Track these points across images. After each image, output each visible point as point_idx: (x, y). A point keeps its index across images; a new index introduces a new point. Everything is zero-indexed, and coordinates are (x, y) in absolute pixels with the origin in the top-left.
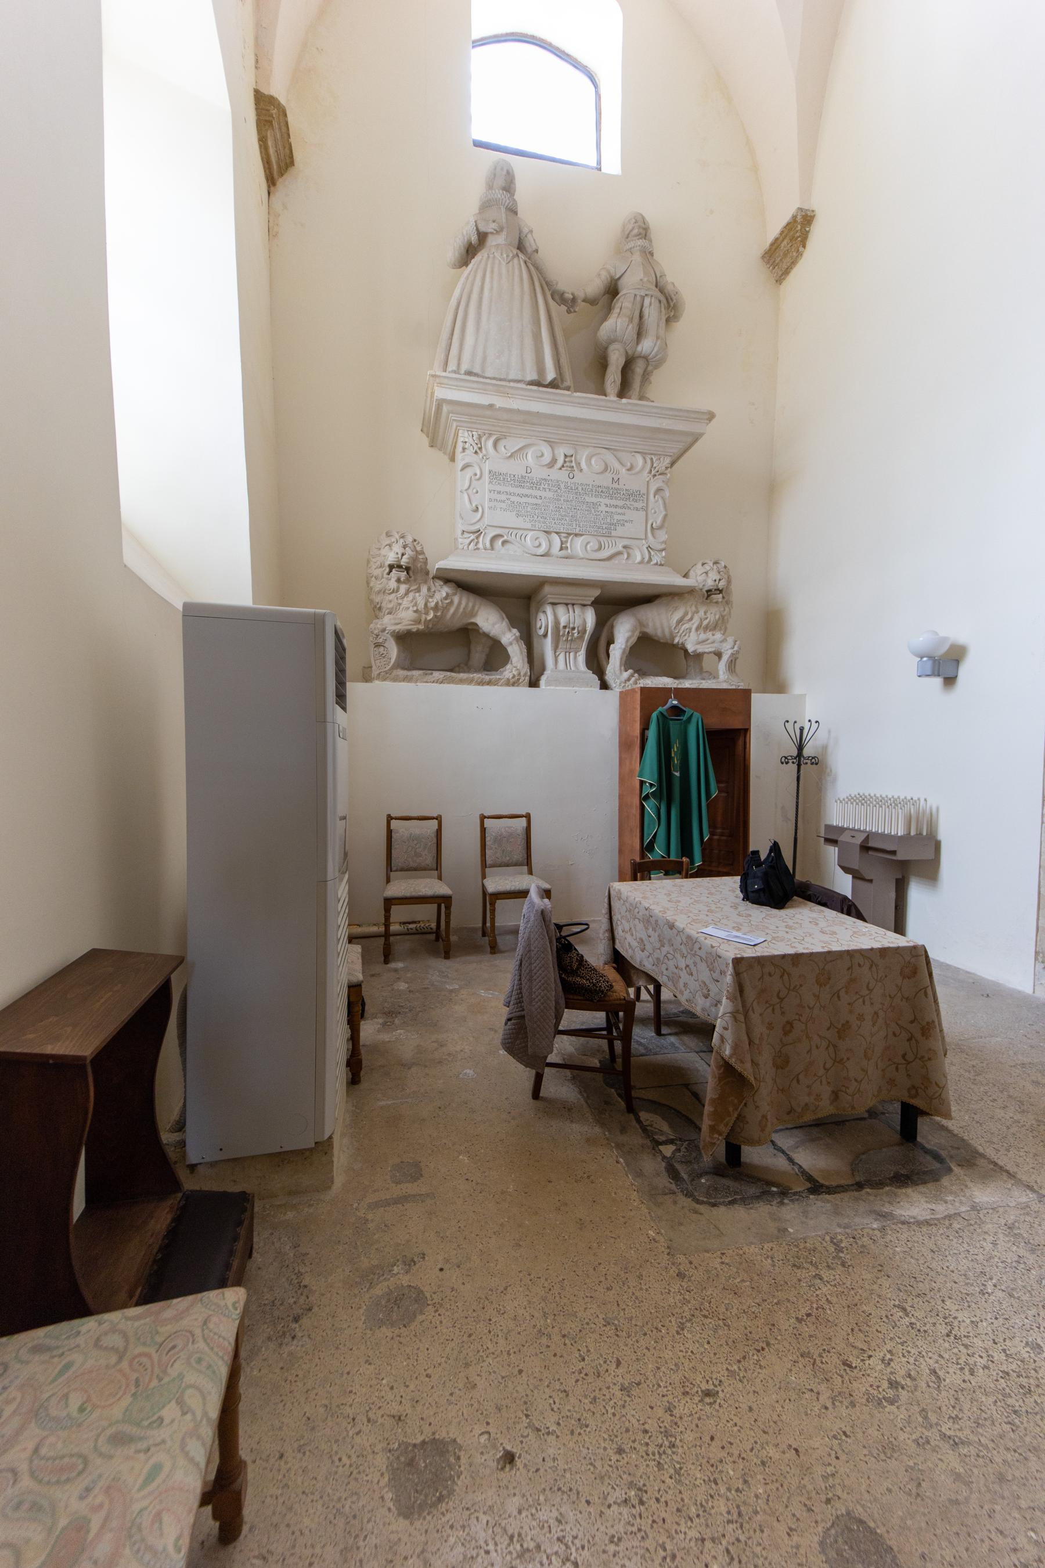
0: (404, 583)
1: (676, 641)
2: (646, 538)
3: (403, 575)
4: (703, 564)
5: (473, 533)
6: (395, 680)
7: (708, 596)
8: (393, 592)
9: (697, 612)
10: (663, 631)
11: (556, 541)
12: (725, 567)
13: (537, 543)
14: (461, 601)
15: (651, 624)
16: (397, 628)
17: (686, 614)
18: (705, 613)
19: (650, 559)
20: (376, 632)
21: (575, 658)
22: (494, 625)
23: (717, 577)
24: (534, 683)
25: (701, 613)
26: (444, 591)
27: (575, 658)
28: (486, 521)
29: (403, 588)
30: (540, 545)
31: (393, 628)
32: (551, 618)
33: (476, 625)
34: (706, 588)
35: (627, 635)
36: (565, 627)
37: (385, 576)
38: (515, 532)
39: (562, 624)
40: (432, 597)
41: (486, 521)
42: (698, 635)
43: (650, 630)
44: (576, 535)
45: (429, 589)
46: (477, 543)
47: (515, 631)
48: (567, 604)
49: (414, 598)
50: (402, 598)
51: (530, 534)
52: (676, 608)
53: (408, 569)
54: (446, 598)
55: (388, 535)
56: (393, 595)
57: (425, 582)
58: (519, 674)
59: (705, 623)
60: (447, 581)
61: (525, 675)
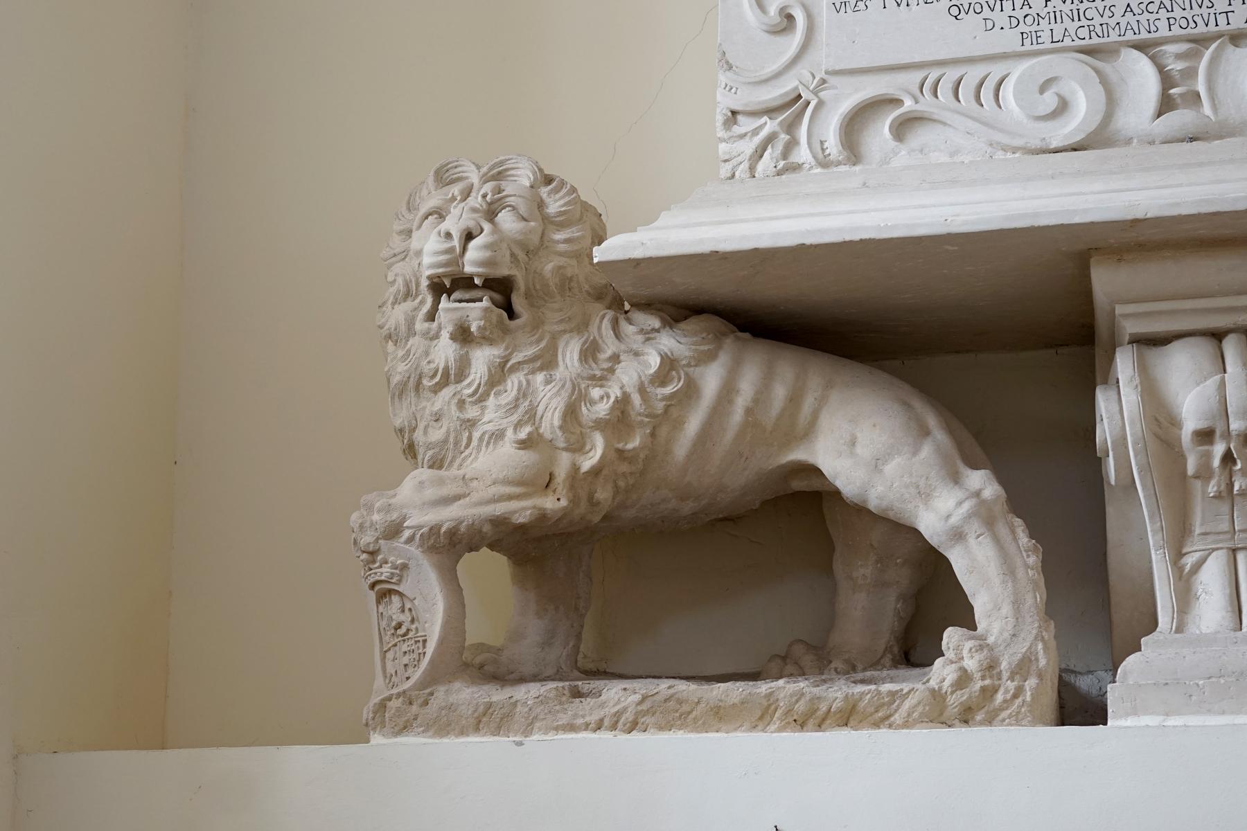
0: (486, 339)
3: (477, 311)
5: (771, 111)
6: (444, 725)
8: (445, 381)
11: (1141, 78)
13: (1049, 101)
14: (734, 386)
16: (447, 515)
20: (367, 539)
22: (877, 465)
24: (1080, 708)
26: (645, 354)
28: (824, 57)
29: (482, 359)
30: (1063, 106)
31: (430, 517)
32: (1130, 396)
33: (815, 471)
36: (1205, 436)
37: (420, 326)
38: (952, 74)
39: (1190, 423)
40: (600, 380)
41: (824, 57)
45: (590, 352)
46: (791, 145)
47: (981, 481)
48: (1217, 336)
49: (523, 393)
50: (480, 398)
51: (1018, 70)
53: (500, 289)
54: (662, 377)
55: (444, 177)
56: (447, 392)
57: (582, 326)
58: (991, 667)
60: (679, 310)
61: (1023, 668)
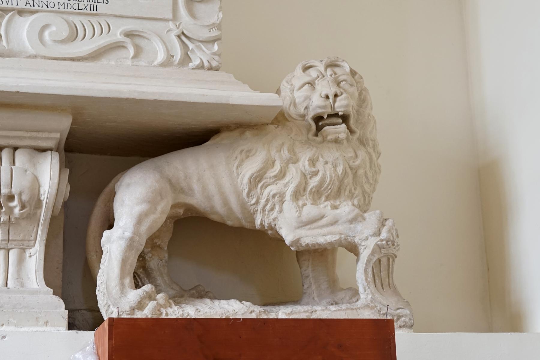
1: (258, 223)
2: (175, 17)
4: (306, 69)
7: (319, 129)
9: (295, 161)
10: (226, 203)
12: (353, 73)
15: (196, 187)
17: (269, 164)
18: (313, 162)
19: (186, 58)
21: (21, 261)
23: (331, 91)
25: (304, 163)
27: (21, 261)
34: (311, 114)
35: (138, 209)
42: (300, 209)
43: (197, 200)
44: (21, 12)
52: (248, 154)
59: (314, 182)
